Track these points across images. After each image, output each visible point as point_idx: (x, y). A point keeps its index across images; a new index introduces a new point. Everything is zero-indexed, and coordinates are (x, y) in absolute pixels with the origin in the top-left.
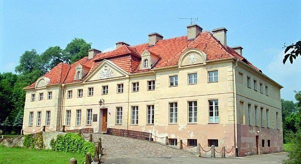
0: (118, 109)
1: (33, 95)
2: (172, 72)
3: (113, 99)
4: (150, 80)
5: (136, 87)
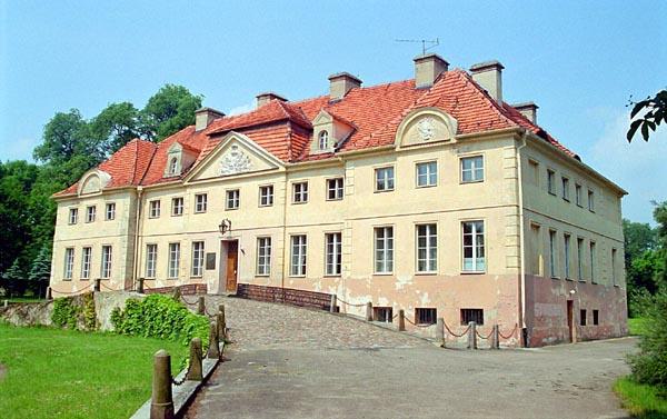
0: (262, 241)
1: (74, 211)
2: (381, 159)
3: (250, 220)
4: (332, 177)
5: (300, 193)
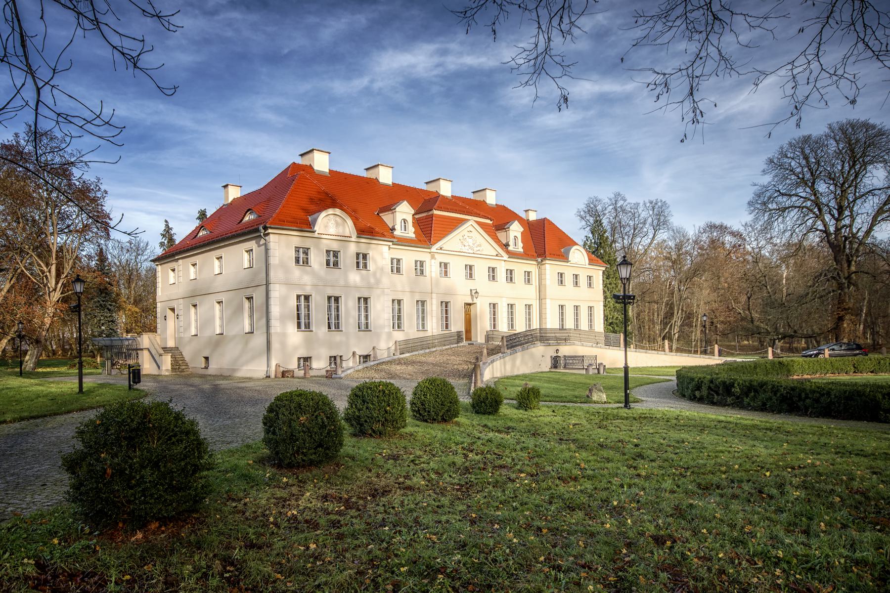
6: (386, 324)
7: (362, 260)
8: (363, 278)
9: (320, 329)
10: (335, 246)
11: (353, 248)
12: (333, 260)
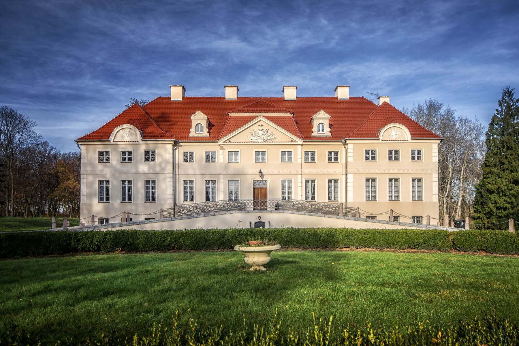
5: (310, 157)
6: (168, 197)
7: (149, 156)
8: (150, 168)
9: (116, 202)
10: (129, 148)
11: (143, 148)
12: (127, 157)
